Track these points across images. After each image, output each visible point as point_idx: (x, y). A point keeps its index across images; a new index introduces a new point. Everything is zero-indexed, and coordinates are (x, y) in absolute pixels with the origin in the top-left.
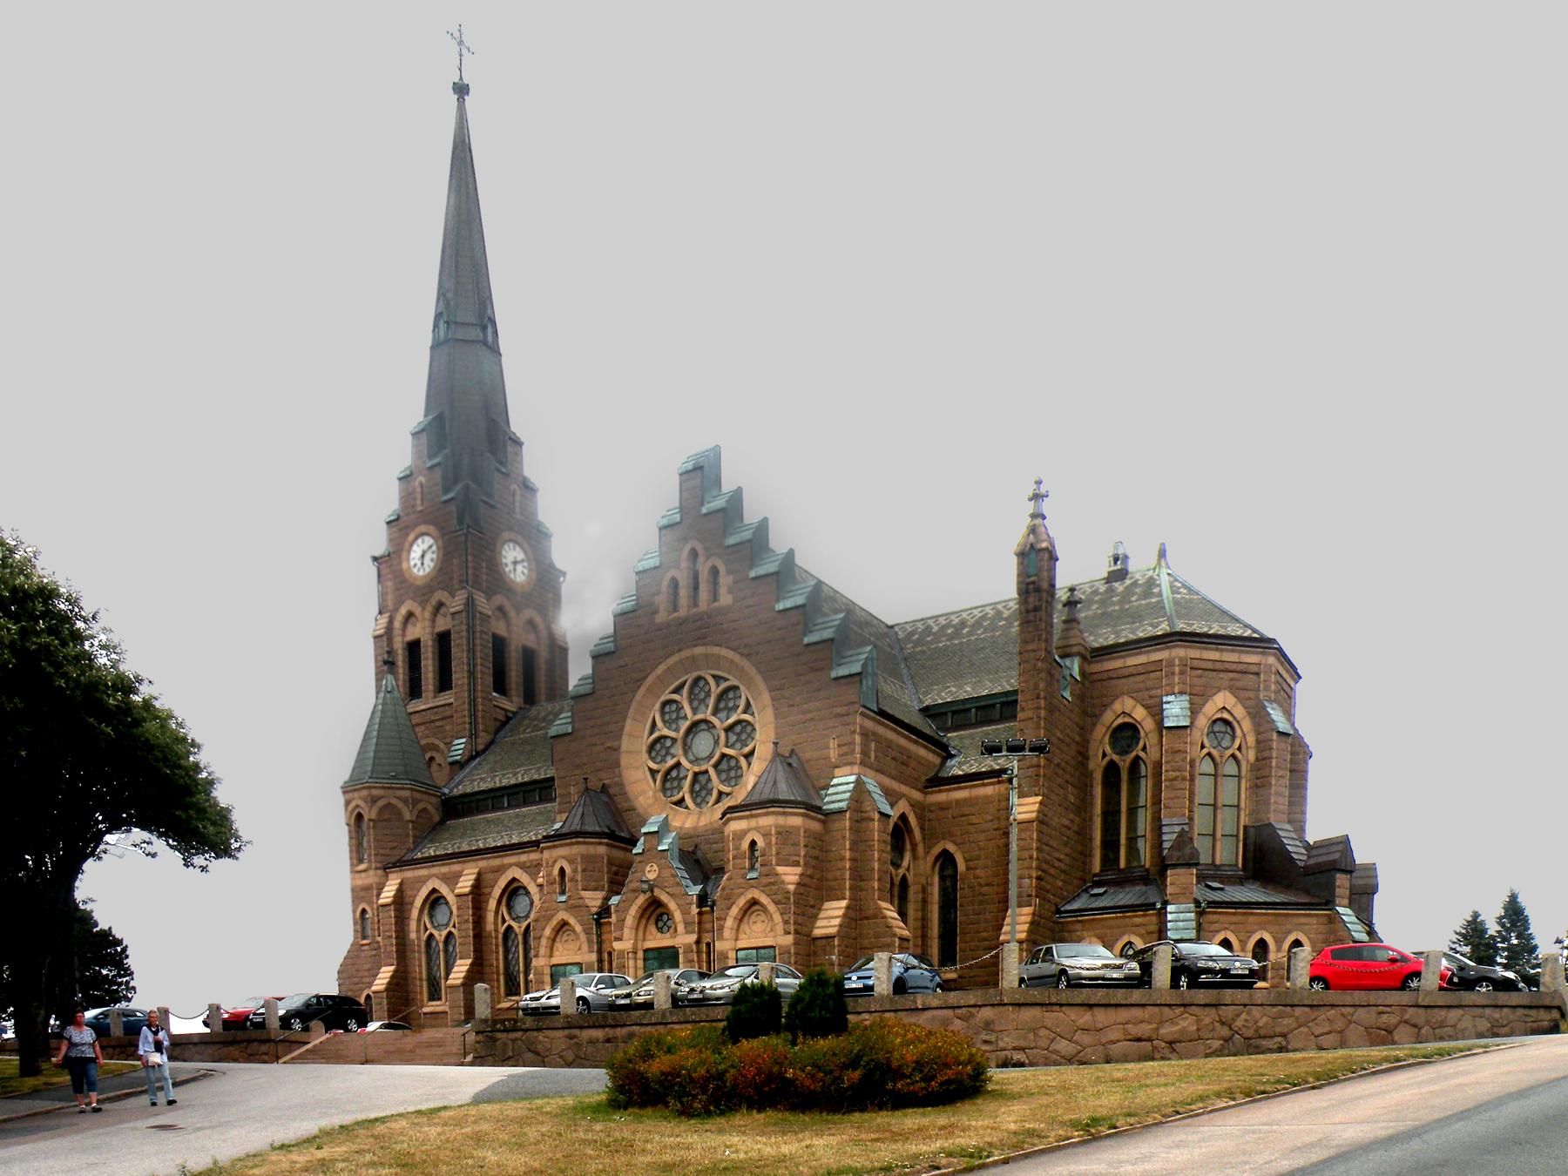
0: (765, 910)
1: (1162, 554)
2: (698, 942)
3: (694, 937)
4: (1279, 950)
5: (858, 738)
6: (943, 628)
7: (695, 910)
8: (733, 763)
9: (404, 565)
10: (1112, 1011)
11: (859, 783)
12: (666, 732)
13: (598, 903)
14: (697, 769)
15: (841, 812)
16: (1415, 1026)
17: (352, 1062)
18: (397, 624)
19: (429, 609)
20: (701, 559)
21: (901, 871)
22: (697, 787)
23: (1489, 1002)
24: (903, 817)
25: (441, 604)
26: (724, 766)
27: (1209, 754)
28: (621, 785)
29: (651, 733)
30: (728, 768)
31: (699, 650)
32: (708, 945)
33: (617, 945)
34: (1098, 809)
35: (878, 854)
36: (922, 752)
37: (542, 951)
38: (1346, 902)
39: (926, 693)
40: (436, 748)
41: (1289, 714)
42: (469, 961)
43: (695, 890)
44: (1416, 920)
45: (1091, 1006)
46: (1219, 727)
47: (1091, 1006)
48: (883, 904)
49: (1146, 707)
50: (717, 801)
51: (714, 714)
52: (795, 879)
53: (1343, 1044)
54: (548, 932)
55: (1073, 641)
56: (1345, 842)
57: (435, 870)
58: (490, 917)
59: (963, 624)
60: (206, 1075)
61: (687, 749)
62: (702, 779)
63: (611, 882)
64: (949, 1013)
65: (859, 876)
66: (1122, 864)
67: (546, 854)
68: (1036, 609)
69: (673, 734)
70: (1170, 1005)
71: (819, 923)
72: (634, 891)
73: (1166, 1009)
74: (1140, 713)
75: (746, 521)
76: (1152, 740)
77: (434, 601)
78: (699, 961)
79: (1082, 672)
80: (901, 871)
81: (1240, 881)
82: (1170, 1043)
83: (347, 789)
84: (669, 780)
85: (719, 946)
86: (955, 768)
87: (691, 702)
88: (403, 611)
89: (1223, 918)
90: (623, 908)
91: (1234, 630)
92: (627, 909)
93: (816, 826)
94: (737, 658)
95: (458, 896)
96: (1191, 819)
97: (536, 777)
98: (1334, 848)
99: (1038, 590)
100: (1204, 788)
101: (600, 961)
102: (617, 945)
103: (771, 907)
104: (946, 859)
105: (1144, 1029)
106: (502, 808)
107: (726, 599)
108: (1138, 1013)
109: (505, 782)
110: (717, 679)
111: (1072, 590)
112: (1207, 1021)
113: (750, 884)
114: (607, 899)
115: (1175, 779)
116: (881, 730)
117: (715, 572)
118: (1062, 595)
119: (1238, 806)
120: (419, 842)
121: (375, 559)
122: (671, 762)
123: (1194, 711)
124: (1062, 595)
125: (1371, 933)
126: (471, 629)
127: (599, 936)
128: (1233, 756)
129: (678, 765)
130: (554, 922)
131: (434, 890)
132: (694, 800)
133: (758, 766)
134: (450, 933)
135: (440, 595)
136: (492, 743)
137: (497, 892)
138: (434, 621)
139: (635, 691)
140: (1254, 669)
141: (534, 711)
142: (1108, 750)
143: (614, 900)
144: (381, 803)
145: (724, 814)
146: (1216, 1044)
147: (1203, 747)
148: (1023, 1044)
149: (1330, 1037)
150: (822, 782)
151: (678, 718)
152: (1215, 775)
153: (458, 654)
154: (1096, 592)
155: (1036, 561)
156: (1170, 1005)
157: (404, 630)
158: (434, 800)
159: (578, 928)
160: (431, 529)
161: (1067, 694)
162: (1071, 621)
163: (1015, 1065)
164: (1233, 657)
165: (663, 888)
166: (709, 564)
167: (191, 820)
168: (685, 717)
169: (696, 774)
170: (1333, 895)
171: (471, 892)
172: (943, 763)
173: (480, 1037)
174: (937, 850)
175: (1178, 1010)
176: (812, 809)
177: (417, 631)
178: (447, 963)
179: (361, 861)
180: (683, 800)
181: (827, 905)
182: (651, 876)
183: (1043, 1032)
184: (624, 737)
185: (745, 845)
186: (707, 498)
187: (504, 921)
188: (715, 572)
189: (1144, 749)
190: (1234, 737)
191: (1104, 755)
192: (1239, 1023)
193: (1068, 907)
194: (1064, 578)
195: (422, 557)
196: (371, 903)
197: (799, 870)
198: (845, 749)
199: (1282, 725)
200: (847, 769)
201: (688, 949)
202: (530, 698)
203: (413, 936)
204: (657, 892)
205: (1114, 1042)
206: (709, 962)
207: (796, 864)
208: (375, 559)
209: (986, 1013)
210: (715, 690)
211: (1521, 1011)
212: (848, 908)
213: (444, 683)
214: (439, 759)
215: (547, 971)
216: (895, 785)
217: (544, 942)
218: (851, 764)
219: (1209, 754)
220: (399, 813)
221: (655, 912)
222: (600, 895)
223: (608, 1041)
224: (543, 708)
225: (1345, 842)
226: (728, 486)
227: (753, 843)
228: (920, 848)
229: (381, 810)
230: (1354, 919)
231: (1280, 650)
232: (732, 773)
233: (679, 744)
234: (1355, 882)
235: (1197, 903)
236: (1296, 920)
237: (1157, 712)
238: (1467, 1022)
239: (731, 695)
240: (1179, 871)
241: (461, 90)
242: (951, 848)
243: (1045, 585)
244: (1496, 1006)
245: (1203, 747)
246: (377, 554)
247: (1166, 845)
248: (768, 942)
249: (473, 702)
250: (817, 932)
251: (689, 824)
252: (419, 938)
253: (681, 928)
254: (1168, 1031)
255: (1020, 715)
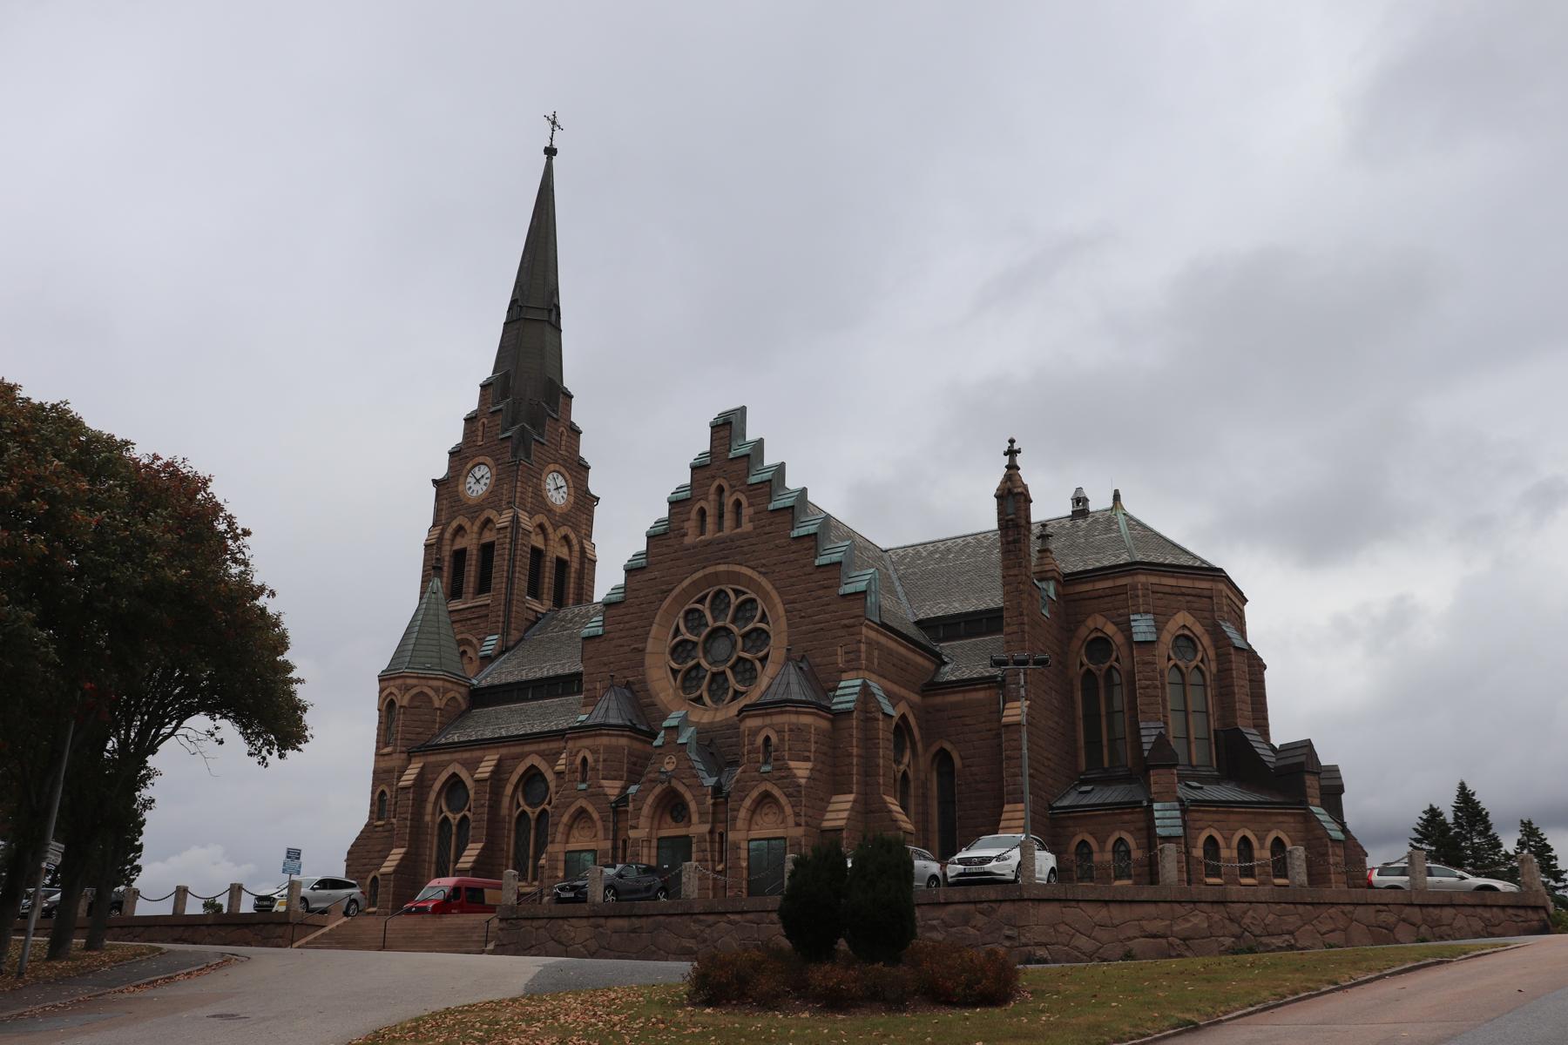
0: (776, 801)
1: (1117, 497)
2: (711, 832)
3: (707, 827)
4: (1262, 847)
5: (863, 647)
6: (931, 553)
7: (709, 801)
8: (748, 666)
9: (460, 488)
10: (1127, 907)
11: (865, 686)
12: (688, 636)
13: (616, 791)
14: (714, 669)
15: (848, 713)
16: (1413, 924)
17: (369, 948)
18: (447, 535)
19: (478, 523)
20: (726, 493)
21: (902, 767)
22: (714, 686)
23: (1478, 902)
24: (903, 717)
25: (489, 521)
26: (740, 668)
27: (1176, 665)
28: (644, 682)
29: (675, 636)
30: (746, 671)
31: (722, 568)
32: (721, 835)
33: (632, 834)
34: (1080, 712)
35: (885, 749)
36: (919, 660)
37: (559, 837)
38: (1317, 801)
39: (920, 608)
40: (469, 643)
41: (1242, 632)
42: (480, 845)
43: (710, 781)
44: (1383, 802)
45: (1106, 902)
46: (1181, 642)
47: (1106, 902)
48: (888, 799)
49: (1115, 624)
50: (733, 699)
51: (733, 622)
52: (806, 773)
53: (1348, 942)
54: (565, 819)
55: (1048, 568)
56: (1307, 746)
57: (457, 756)
58: (506, 801)
59: (949, 550)
60: (226, 961)
61: (706, 652)
62: (720, 679)
63: (630, 771)
64: (971, 907)
65: (869, 770)
66: (1106, 765)
67: (570, 744)
68: (1015, 541)
69: (694, 638)
70: (1179, 902)
71: (828, 816)
72: (651, 781)
73: (1176, 906)
74: (1110, 629)
75: (766, 463)
76: (1124, 651)
77: (482, 518)
78: (712, 851)
79: (1057, 594)
80: (902, 767)
81: (1217, 781)
82: (1184, 939)
83: (384, 678)
84: (689, 680)
85: (731, 836)
86: (949, 673)
87: (712, 612)
88: (454, 524)
89: (1206, 816)
90: (640, 798)
91: (1184, 560)
92: (644, 799)
93: (824, 724)
94: (755, 575)
95: (477, 781)
96: (1166, 723)
97: (560, 672)
98: (1299, 752)
99: (1017, 526)
100: (1172, 696)
101: (615, 848)
102: (632, 834)
103: (783, 800)
104: (943, 758)
105: (1158, 926)
106: (527, 700)
107: (747, 526)
108: (1151, 909)
109: (531, 676)
110: (737, 593)
111: (1044, 525)
112: (1217, 917)
113: (764, 778)
114: (625, 788)
115: (1147, 687)
116: (883, 640)
117: (738, 504)
118: (1036, 530)
119: (1207, 712)
120: (445, 727)
121: (435, 481)
122: (691, 663)
123: (1159, 629)
124: (1036, 530)
125: (1344, 830)
126: (514, 541)
127: (615, 823)
128: (1197, 667)
129: (698, 666)
130: (572, 809)
131: (454, 775)
132: (711, 697)
133: (771, 668)
134: (465, 817)
135: (492, 514)
136: (522, 639)
137: (514, 778)
138: (480, 533)
139: (662, 601)
140: (1206, 593)
141: (561, 614)
142: (1085, 660)
143: (633, 789)
144: (414, 691)
145: (741, 711)
146: (1228, 941)
147: (1169, 659)
148: (1044, 939)
149: (1337, 934)
150: (831, 685)
151: (700, 625)
152: (1184, 684)
153: (500, 563)
154: (1063, 527)
155: (1013, 497)
156: (1179, 902)
157: (453, 540)
158: (463, 690)
159: (595, 816)
160: (488, 460)
161: (1045, 612)
162: (1044, 551)
163: (1038, 962)
164: (1188, 583)
165: (679, 779)
166: (734, 498)
167: (273, 718)
168: (706, 625)
169: (714, 675)
170: (1304, 795)
171: (491, 777)
172: (937, 670)
173: (504, 925)
174: (934, 749)
175: (1189, 907)
176: (822, 709)
177: (469, 542)
178: (457, 846)
179: (387, 745)
180: (701, 697)
181: (835, 798)
182: (670, 767)
183: (1062, 928)
184: (650, 641)
185: (760, 740)
186: (734, 446)
187: (519, 805)
188: (738, 504)
189: (1117, 660)
190: (1196, 650)
191: (1082, 665)
192: (1247, 921)
193: (1059, 804)
194: (1038, 514)
195: (478, 484)
196: (390, 785)
197: (809, 765)
198: (852, 656)
199: (1238, 642)
200: (854, 674)
201: (702, 839)
202: (559, 601)
203: (428, 818)
204: (674, 783)
205: (1129, 939)
206: (721, 852)
207: (807, 759)
208: (435, 481)
209: (1007, 908)
210: (734, 601)
211: (1510, 911)
212: (855, 801)
213: (484, 586)
214: (470, 653)
215: (562, 857)
216: (896, 689)
217: (561, 828)
218: (858, 669)
219: (1176, 665)
220: (430, 700)
221: (673, 806)
222: (619, 784)
223: (634, 931)
224: (571, 611)
225: (1307, 746)
226: (751, 435)
227: (767, 739)
228: (919, 746)
229: (413, 698)
230: (1327, 818)
231: (1228, 578)
232: (747, 675)
233: (700, 647)
234: (1324, 783)
235: (1180, 801)
236: (1274, 818)
237: (1127, 630)
238: (1460, 922)
239: (748, 606)
240: (1161, 771)
241: (550, 152)
242: (948, 746)
243: (1023, 522)
244: (1485, 906)
245: (1169, 659)
246: (439, 477)
247: (1146, 747)
248: (779, 832)
249: (509, 603)
250: (826, 824)
251: (705, 719)
252: (433, 821)
253: (695, 818)
254: (1180, 927)
255: (1006, 629)
